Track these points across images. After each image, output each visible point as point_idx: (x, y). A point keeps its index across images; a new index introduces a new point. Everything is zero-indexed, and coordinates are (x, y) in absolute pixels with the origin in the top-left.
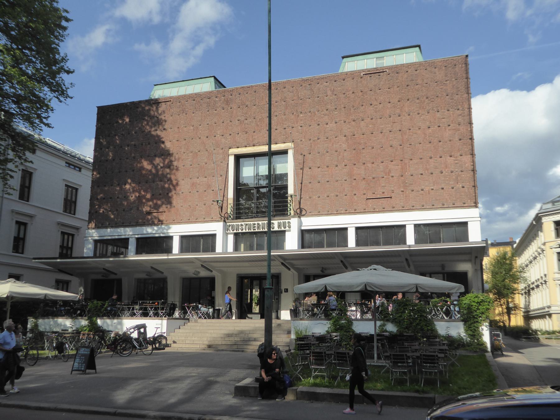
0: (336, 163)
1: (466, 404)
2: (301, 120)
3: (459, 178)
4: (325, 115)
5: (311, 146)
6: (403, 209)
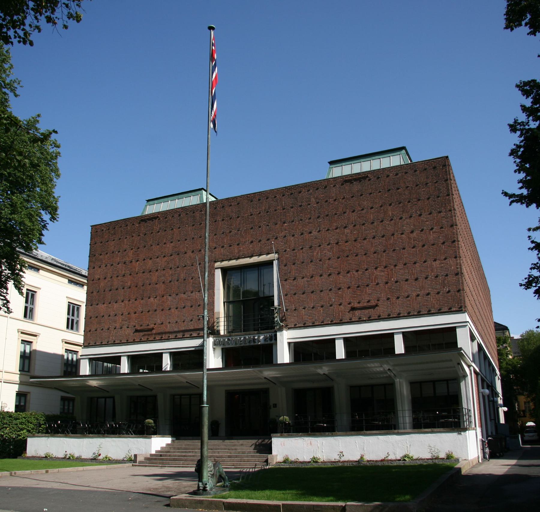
0: (321, 272)
1: (189, 493)
2: (285, 230)
3: (446, 282)
4: (309, 223)
5: (296, 256)
6: (389, 318)
